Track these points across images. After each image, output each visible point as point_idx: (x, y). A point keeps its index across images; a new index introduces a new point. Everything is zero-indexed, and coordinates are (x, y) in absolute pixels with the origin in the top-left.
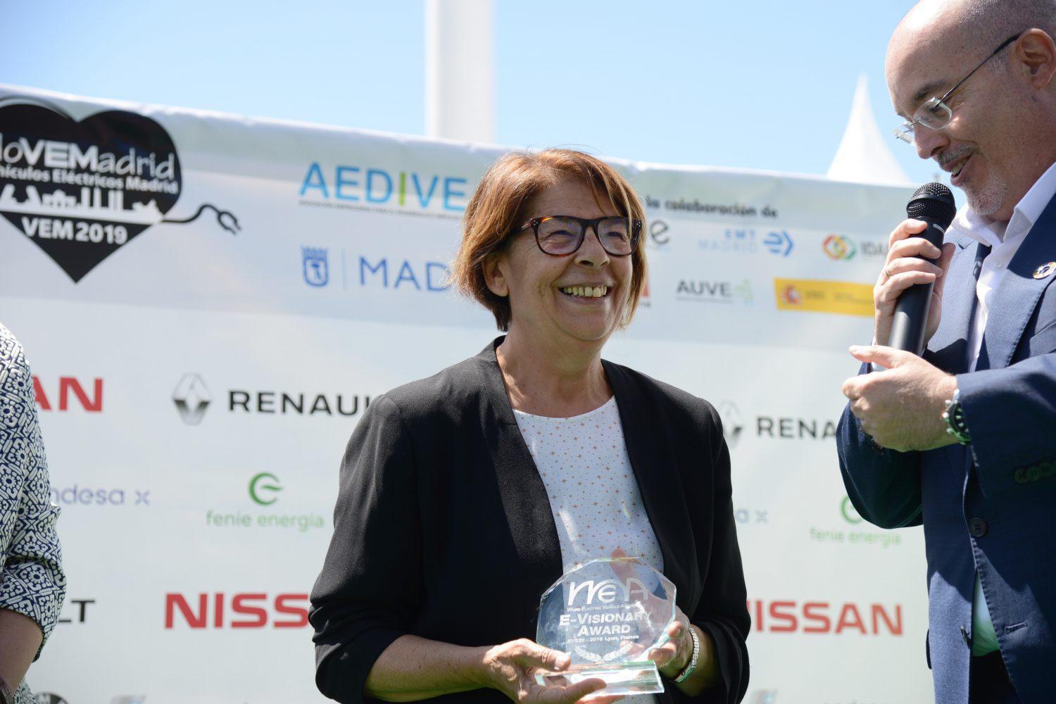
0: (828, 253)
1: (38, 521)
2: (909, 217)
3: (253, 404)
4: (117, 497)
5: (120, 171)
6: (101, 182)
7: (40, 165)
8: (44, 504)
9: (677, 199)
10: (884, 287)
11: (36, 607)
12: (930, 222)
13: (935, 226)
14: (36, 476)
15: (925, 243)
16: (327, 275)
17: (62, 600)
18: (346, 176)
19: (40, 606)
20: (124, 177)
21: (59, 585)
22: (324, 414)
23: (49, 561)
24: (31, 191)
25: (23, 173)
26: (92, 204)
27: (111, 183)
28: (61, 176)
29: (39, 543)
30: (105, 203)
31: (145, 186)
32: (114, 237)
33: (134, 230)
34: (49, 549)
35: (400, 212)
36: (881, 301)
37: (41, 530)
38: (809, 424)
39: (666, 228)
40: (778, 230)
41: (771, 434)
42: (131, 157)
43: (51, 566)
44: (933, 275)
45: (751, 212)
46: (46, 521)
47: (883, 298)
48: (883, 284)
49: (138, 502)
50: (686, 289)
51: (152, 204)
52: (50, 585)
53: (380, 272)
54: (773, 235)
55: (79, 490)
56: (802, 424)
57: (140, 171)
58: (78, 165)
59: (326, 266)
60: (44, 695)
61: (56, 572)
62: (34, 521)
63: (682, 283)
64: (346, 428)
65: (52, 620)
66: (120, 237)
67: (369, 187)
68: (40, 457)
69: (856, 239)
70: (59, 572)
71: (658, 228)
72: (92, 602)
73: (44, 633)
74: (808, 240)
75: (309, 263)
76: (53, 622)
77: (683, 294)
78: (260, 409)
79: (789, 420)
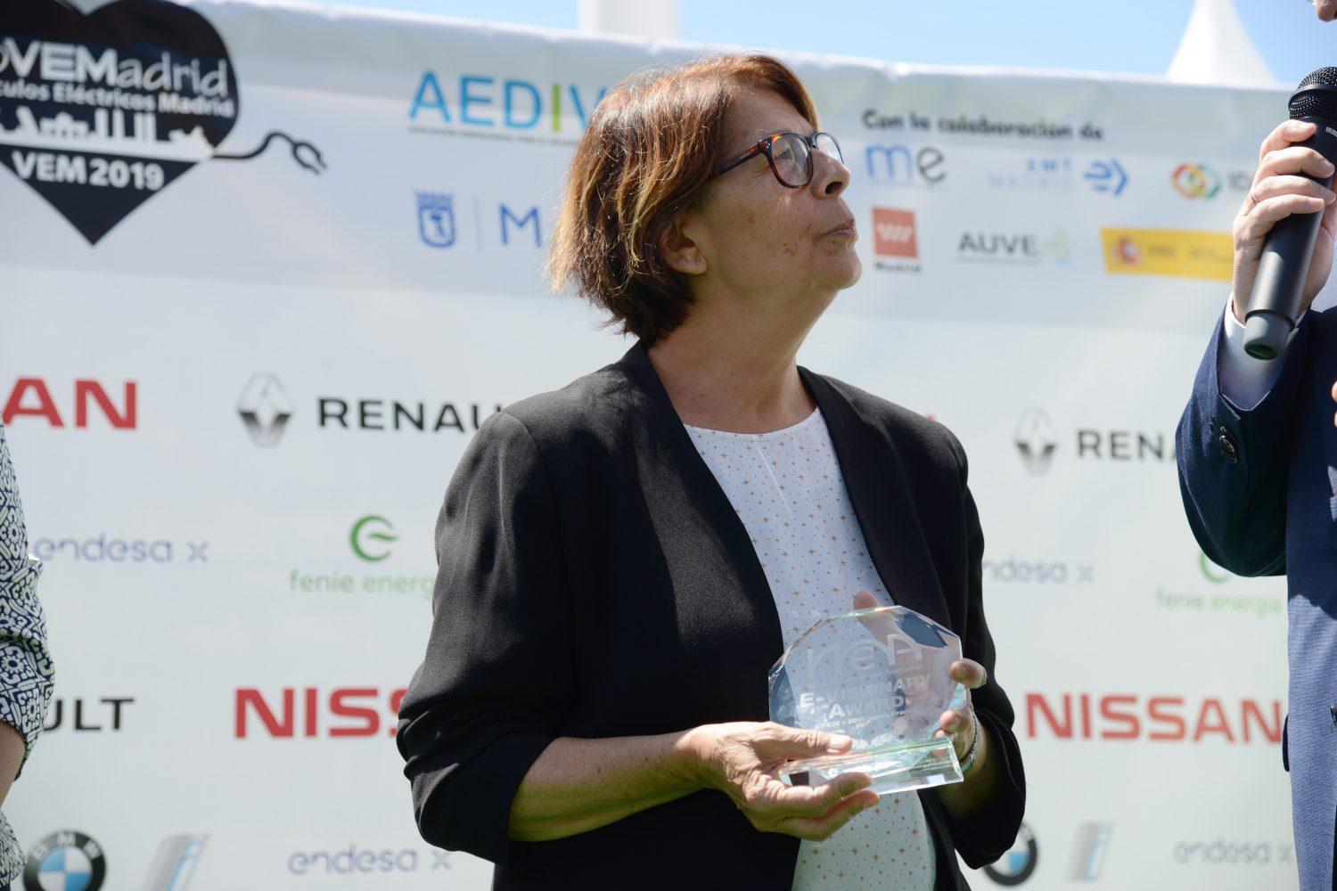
0: (1180, 189)
1: (11, 584)
2: (1291, 118)
3: (353, 417)
4: (161, 551)
5: (150, 86)
6: (123, 100)
7: (35, 77)
8: (19, 558)
9: (955, 116)
10: (1247, 218)
11: (14, 707)
12: (1322, 125)
13: (1329, 130)
14: (7, 518)
15: (1311, 155)
16: (453, 231)
17: (50, 695)
18: (475, 90)
19: (20, 706)
20: (156, 94)
21: (44, 674)
22: (454, 431)
23: (29, 641)
24: (24, 114)
25: (11, 88)
26: (111, 132)
27: (137, 102)
28: (65, 93)
29: (14, 615)
30: (130, 131)
31: (186, 106)
32: (145, 180)
33: (173, 170)
34: (29, 622)
35: (555, 142)
36: (1243, 238)
37: (16, 595)
38: (1152, 438)
39: (940, 159)
40: (1104, 157)
41: (1098, 454)
42: (165, 64)
43: (33, 647)
44: (1320, 200)
45: (1063, 132)
46: (22, 583)
47: (1246, 234)
48: (1246, 215)
49: (192, 558)
50: (972, 246)
51: (198, 133)
52: (32, 674)
53: (530, 226)
54: (1098, 165)
55: (107, 541)
56: (1142, 440)
57: (178, 85)
58: (89, 77)
59: (452, 218)
60: (66, 833)
61: (39, 656)
62: (6, 583)
63: (966, 238)
64: (455, 447)
65: (37, 724)
66: (154, 180)
67: (508, 106)
68: (11, 492)
69: (1221, 168)
70: (44, 656)
71: (928, 159)
72: (130, 700)
73: (26, 743)
74: (1149, 172)
75: (427, 214)
76: (38, 727)
77: (968, 252)
78: (363, 425)
79: (1124, 434)
